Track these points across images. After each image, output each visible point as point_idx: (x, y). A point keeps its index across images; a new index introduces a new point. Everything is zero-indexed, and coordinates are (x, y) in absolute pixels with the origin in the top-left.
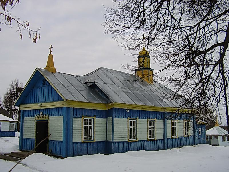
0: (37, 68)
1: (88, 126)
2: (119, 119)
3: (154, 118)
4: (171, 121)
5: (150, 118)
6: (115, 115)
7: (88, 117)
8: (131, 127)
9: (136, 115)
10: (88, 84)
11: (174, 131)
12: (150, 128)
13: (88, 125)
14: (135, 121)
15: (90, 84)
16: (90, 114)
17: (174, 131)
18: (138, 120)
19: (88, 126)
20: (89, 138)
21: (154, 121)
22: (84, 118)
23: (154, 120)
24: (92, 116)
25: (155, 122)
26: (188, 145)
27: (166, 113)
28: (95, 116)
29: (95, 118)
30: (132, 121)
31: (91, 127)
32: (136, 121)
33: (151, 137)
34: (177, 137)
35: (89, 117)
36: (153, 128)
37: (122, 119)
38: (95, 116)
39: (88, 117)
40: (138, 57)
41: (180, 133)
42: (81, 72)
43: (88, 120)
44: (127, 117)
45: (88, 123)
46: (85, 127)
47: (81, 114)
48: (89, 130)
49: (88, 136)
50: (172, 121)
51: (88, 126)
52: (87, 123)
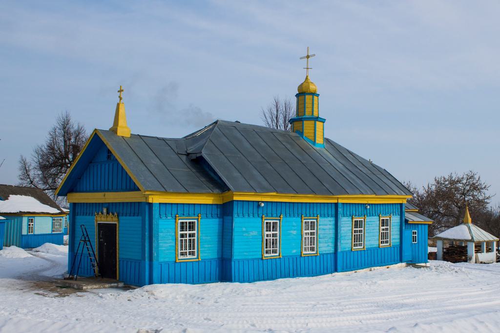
0: (96, 129)
1: (188, 232)
2: (246, 219)
3: (316, 215)
4: (352, 218)
5: (308, 215)
6: (236, 212)
7: (187, 218)
8: (268, 233)
9: (279, 211)
10: (190, 155)
11: (357, 239)
12: (383, 230)
13: (186, 231)
14: (314, 221)
15: (194, 157)
16: (191, 212)
17: (357, 239)
18: (319, 219)
19: (186, 234)
20: (190, 254)
21: (278, 221)
22: (179, 219)
23: (315, 219)
24: (194, 214)
25: (317, 222)
26: (381, 262)
27: (340, 206)
28: (177, 216)
29: (199, 219)
30: (270, 223)
31: (193, 235)
32: (278, 221)
33: (308, 249)
34: (364, 248)
35: (189, 218)
36: (360, 231)
37: (252, 219)
38: (200, 215)
39: (187, 218)
40: (297, 96)
41: (371, 239)
42: (179, 132)
43: (186, 223)
44: (260, 215)
45: (186, 228)
46: (182, 236)
47: (174, 212)
48: (190, 240)
49: (271, 249)
50: (381, 219)
51: (186, 234)
52: (185, 228)
